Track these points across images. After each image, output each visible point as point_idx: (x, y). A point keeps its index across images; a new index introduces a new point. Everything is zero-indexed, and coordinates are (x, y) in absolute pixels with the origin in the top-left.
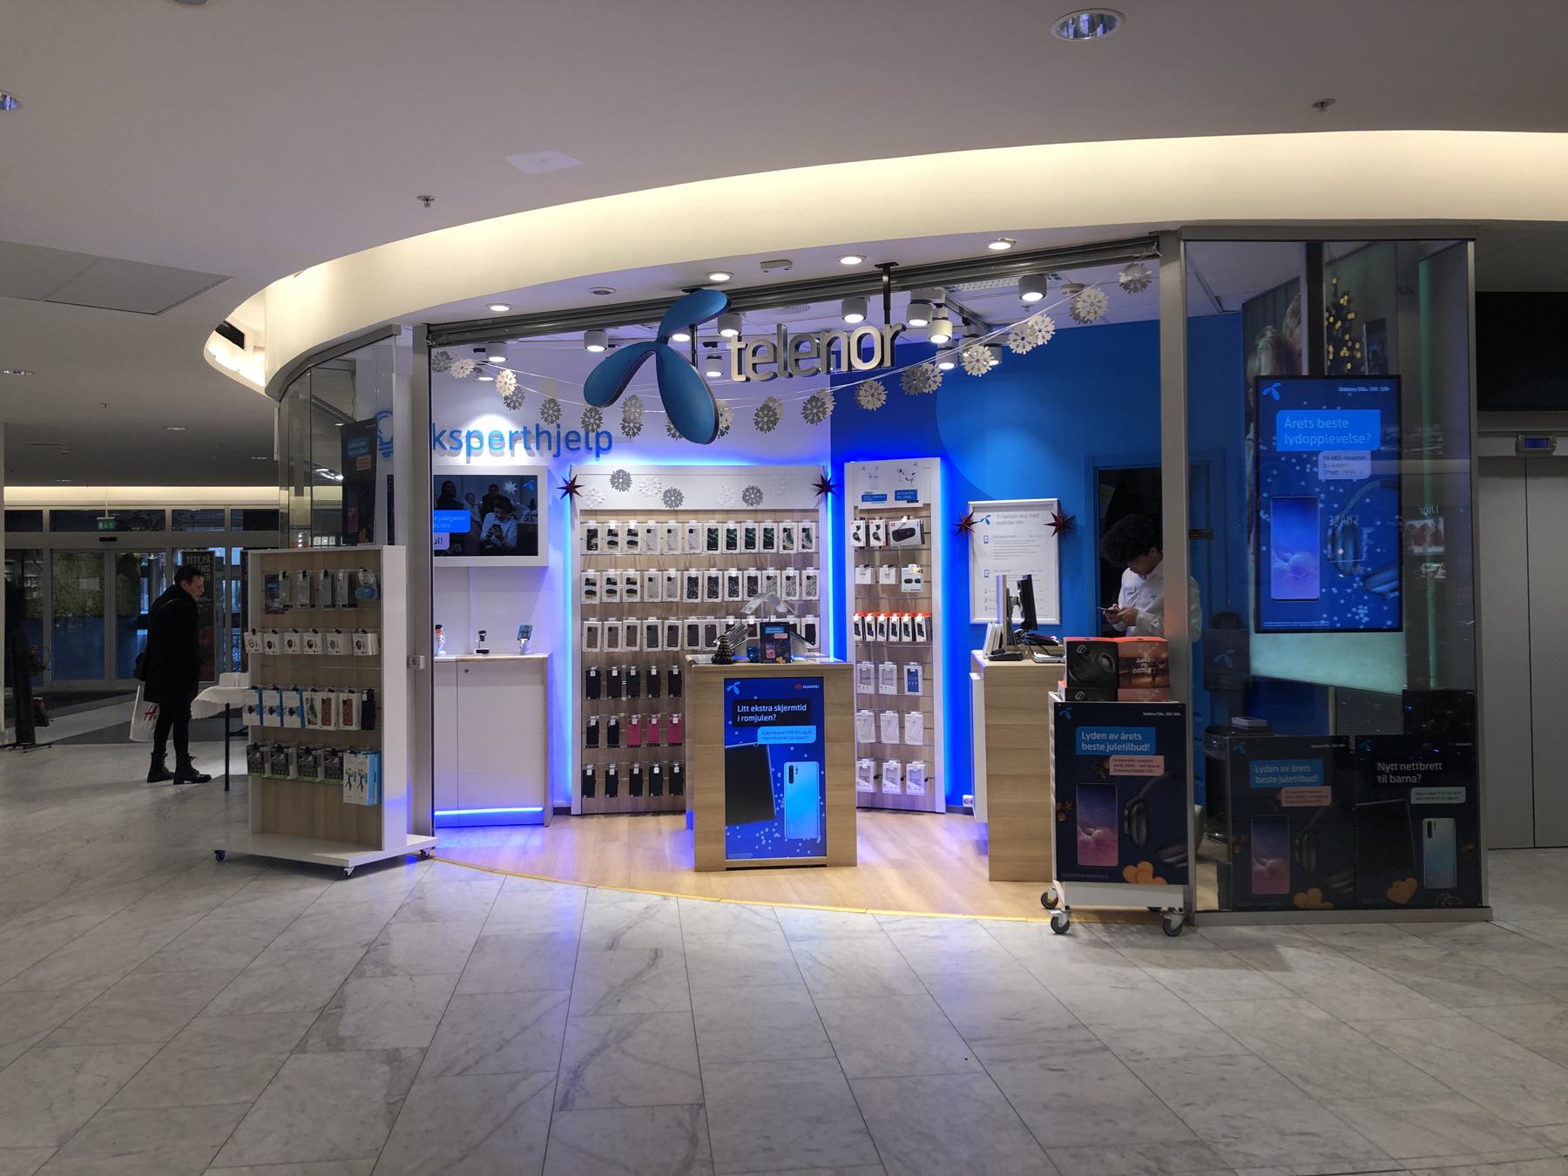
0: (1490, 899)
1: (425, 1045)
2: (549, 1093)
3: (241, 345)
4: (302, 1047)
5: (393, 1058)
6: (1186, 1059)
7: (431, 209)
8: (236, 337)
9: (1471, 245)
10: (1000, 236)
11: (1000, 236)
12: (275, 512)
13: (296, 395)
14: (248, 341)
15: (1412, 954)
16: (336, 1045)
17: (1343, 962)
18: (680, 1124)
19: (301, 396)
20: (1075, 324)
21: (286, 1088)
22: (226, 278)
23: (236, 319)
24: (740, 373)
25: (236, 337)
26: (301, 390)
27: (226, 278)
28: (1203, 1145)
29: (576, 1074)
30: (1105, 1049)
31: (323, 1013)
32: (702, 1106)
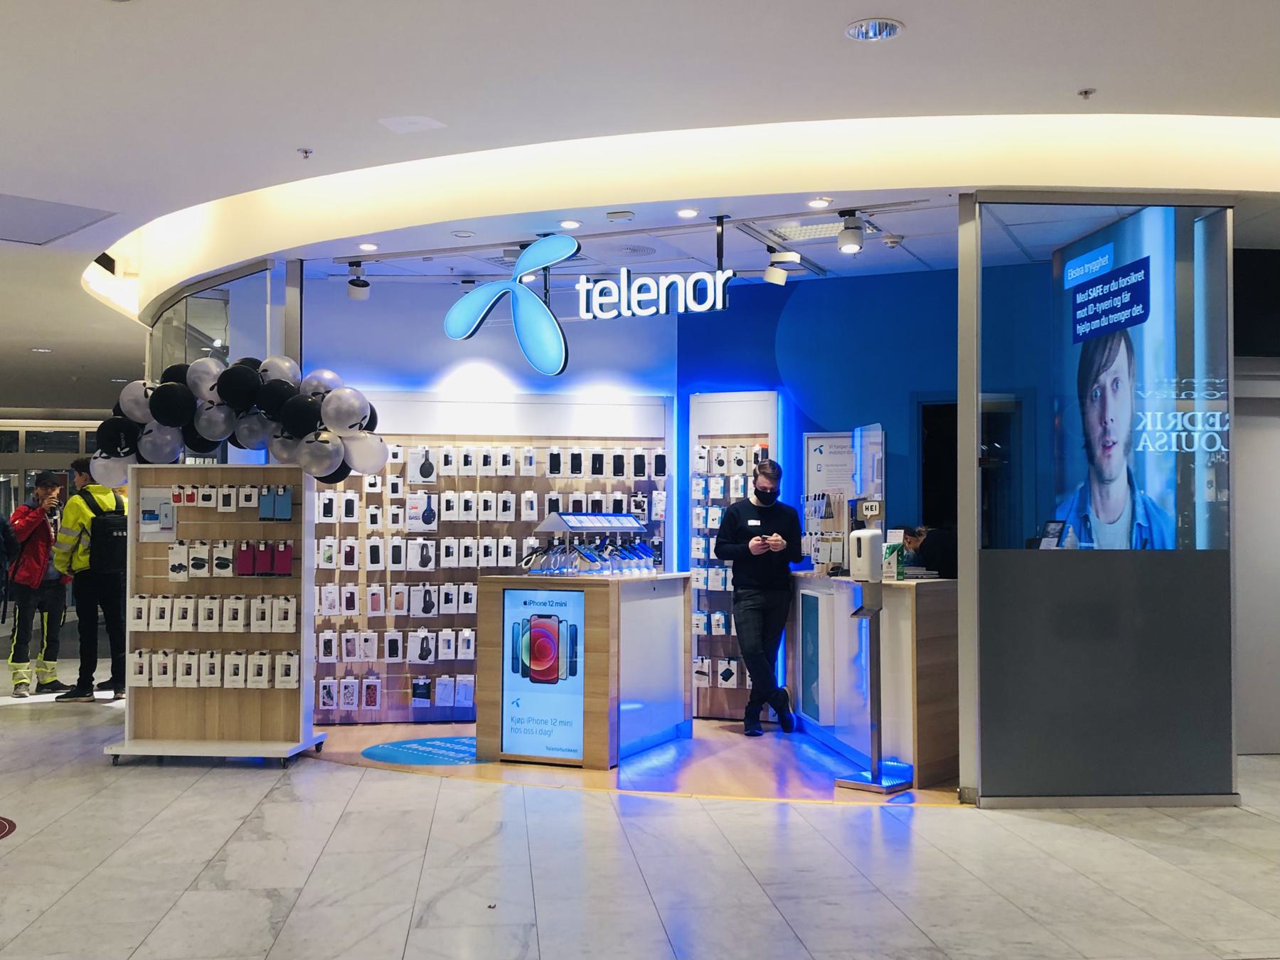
0: (1239, 786)
1: (300, 885)
2: (407, 917)
3: (113, 272)
4: (194, 886)
5: (271, 894)
6: (942, 897)
7: (306, 159)
8: (107, 263)
9: (1230, 212)
10: (820, 196)
11: (820, 196)
12: (984, 269)
13: (169, 321)
14: (118, 267)
15: (1160, 830)
16: (225, 886)
17: (1101, 835)
18: (515, 936)
19: (175, 323)
20: (925, 269)
21: (185, 912)
22: (112, 215)
23: (110, 252)
24: (588, 311)
25: (107, 263)
26: (176, 316)
27: (112, 215)
28: (941, 951)
29: (429, 906)
30: (878, 890)
31: (208, 864)
32: (534, 925)
